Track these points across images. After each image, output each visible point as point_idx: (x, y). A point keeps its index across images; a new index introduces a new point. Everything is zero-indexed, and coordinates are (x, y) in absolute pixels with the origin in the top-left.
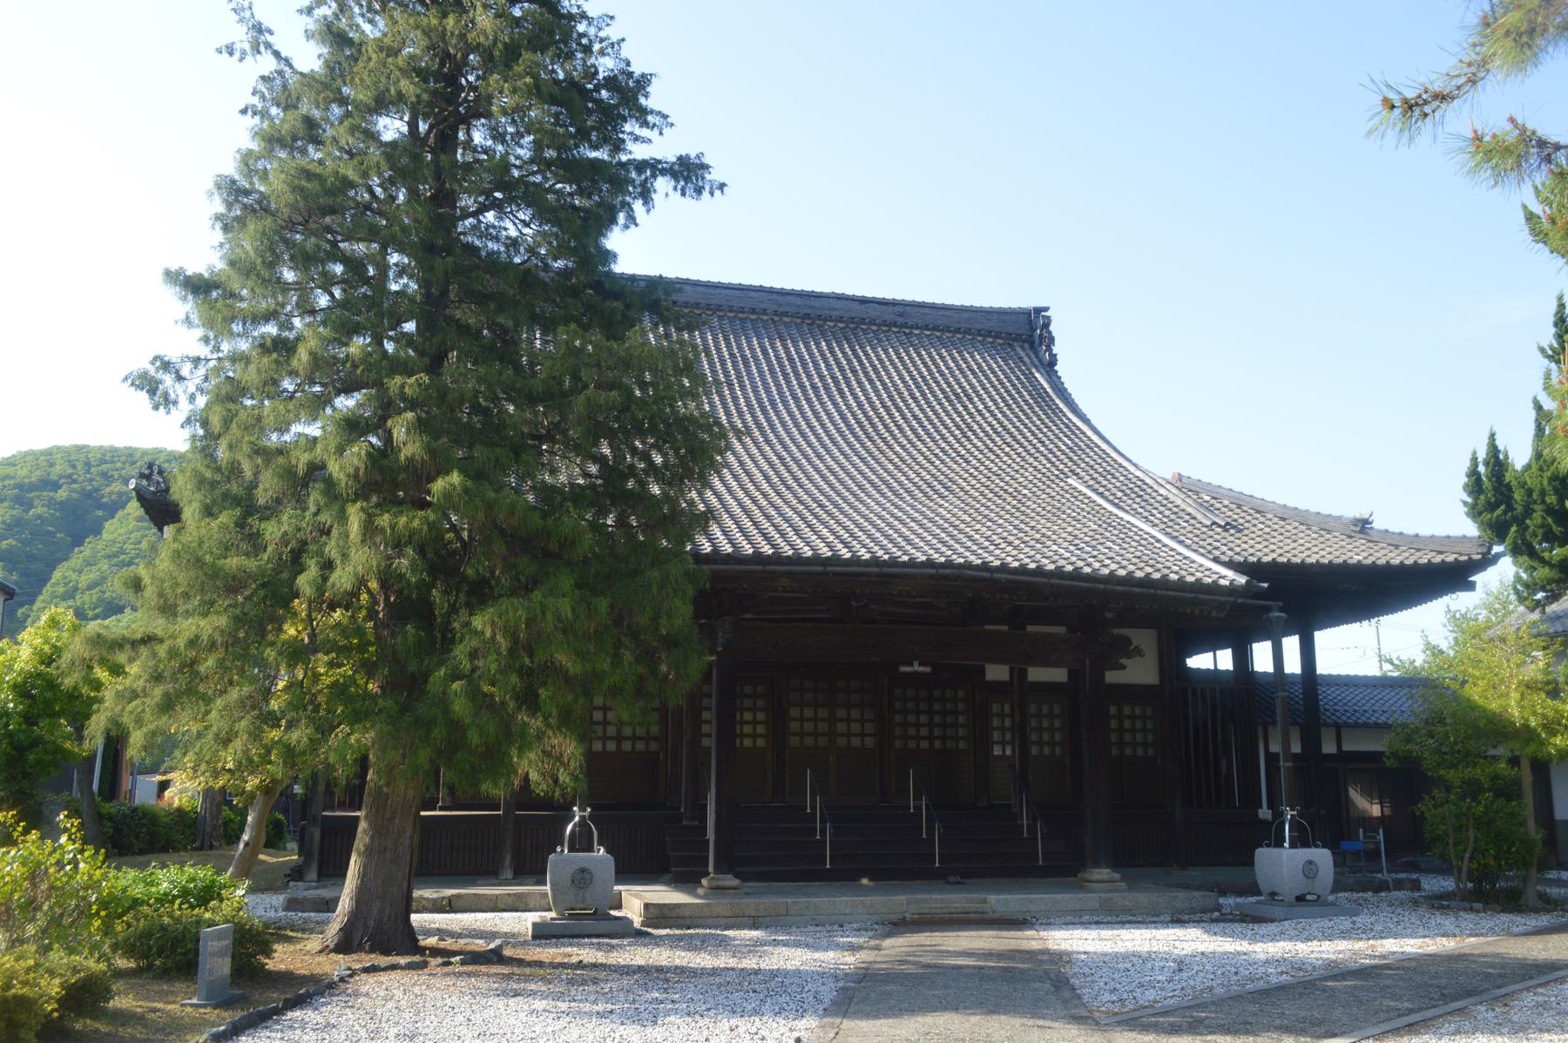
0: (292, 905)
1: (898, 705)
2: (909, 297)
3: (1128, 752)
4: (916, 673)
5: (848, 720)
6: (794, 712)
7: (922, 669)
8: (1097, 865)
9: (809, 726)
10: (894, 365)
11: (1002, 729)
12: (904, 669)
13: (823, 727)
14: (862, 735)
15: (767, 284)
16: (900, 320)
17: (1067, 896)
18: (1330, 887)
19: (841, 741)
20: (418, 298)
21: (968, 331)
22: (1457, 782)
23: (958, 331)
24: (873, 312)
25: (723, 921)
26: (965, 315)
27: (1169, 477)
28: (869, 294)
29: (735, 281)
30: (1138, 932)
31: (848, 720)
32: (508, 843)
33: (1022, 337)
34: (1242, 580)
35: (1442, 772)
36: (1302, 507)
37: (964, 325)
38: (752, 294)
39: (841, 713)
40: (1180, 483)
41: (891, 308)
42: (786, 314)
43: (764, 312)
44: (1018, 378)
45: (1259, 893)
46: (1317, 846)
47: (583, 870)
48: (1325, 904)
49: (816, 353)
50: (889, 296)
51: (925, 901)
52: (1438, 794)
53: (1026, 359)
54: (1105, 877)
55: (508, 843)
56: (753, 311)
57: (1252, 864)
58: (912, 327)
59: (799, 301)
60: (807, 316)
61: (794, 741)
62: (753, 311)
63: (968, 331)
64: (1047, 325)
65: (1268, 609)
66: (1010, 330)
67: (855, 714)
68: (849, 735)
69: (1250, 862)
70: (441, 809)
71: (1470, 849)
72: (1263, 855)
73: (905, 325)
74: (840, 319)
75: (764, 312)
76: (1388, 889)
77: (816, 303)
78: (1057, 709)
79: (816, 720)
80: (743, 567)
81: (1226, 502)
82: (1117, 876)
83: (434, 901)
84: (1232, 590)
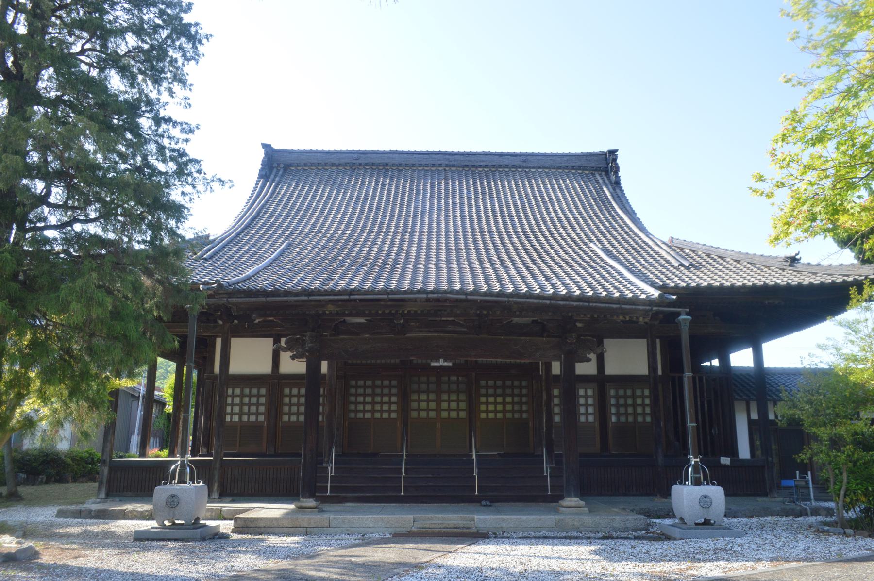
0: (61, 514)
1: (483, 391)
2: (530, 151)
3: (640, 419)
4: (441, 366)
5: (449, 401)
6: (415, 397)
7: (446, 364)
8: (569, 496)
9: (491, 407)
10: (509, 190)
11: (586, 405)
12: (434, 364)
13: (433, 405)
14: (458, 410)
15: (443, 150)
16: (524, 164)
17: (532, 517)
18: (723, 514)
19: (444, 414)
20: (82, 139)
21: (567, 168)
22: (825, 437)
23: (559, 168)
24: (506, 161)
25: (286, 530)
26: (565, 158)
27: (666, 240)
28: (505, 151)
29: (424, 149)
30: (574, 548)
31: (449, 401)
32: (216, 477)
33: (600, 169)
34: (656, 293)
35: (814, 429)
36: (751, 252)
37: (563, 165)
38: (434, 156)
39: (445, 397)
40: (672, 245)
41: (518, 158)
42: (453, 166)
43: (440, 165)
44: (590, 192)
45: (674, 516)
46: (713, 484)
47: (173, 496)
48: (720, 527)
49: (466, 187)
50: (517, 151)
51: (432, 519)
52: (814, 446)
53: (601, 181)
54: (573, 504)
55: (216, 477)
56: (434, 165)
57: (670, 495)
58: (529, 168)
59: (462, 158)
60: (466, 166)
61: (414, 414)
62: (434, 165)
63: (567, 168)
64: (615, 160)
65: (679, 314)
66: (593, 165)
67: (454, 397)
68: (449, 410)
69: (667, 494)
70: (200, 456)
71: (844, 488)
72: (676, 489)
73: (527, 167)
74: (486, 166)
75: (440, 165)
76: (807, 515)
77: (472, 158)
78: (590, 392)
79: (428, 401)
80: (296, 298)
81: (758, 266)
82: (582, 503)
83: (141, 512)
84: (650, 302)
